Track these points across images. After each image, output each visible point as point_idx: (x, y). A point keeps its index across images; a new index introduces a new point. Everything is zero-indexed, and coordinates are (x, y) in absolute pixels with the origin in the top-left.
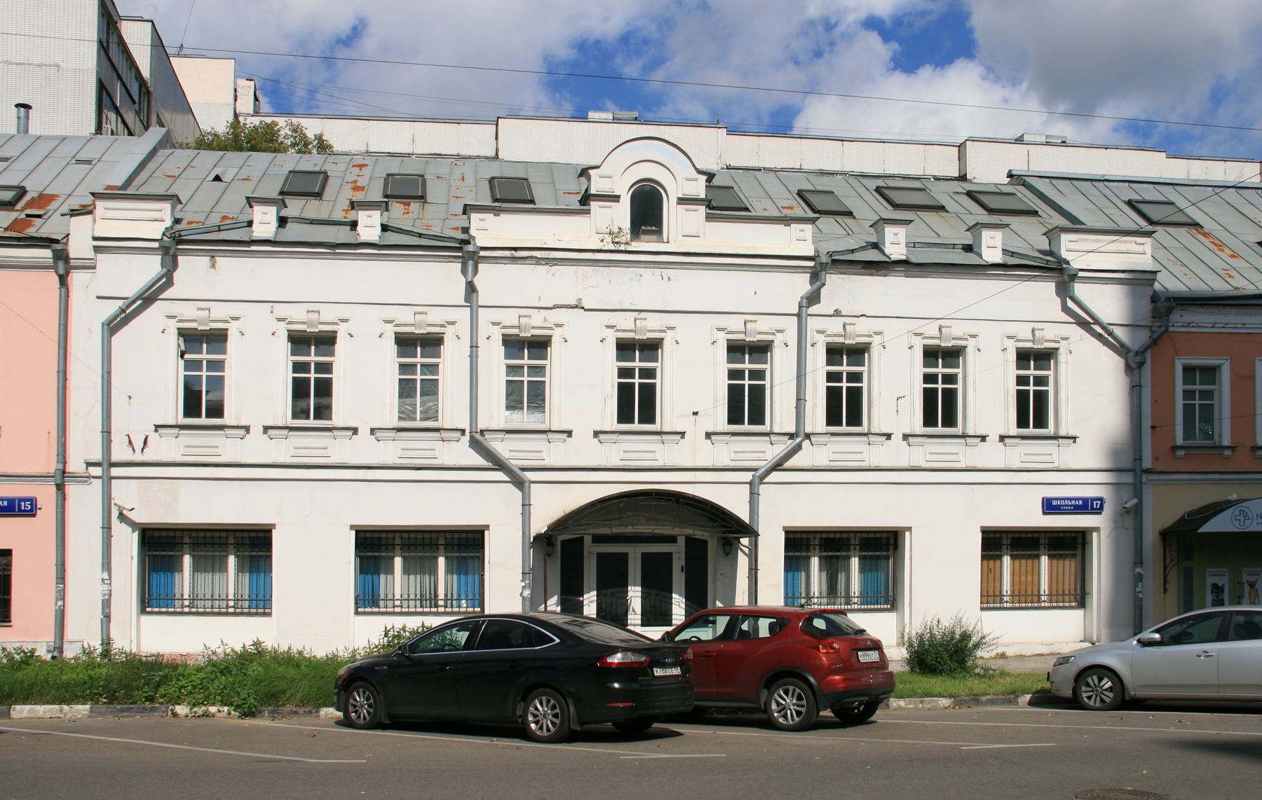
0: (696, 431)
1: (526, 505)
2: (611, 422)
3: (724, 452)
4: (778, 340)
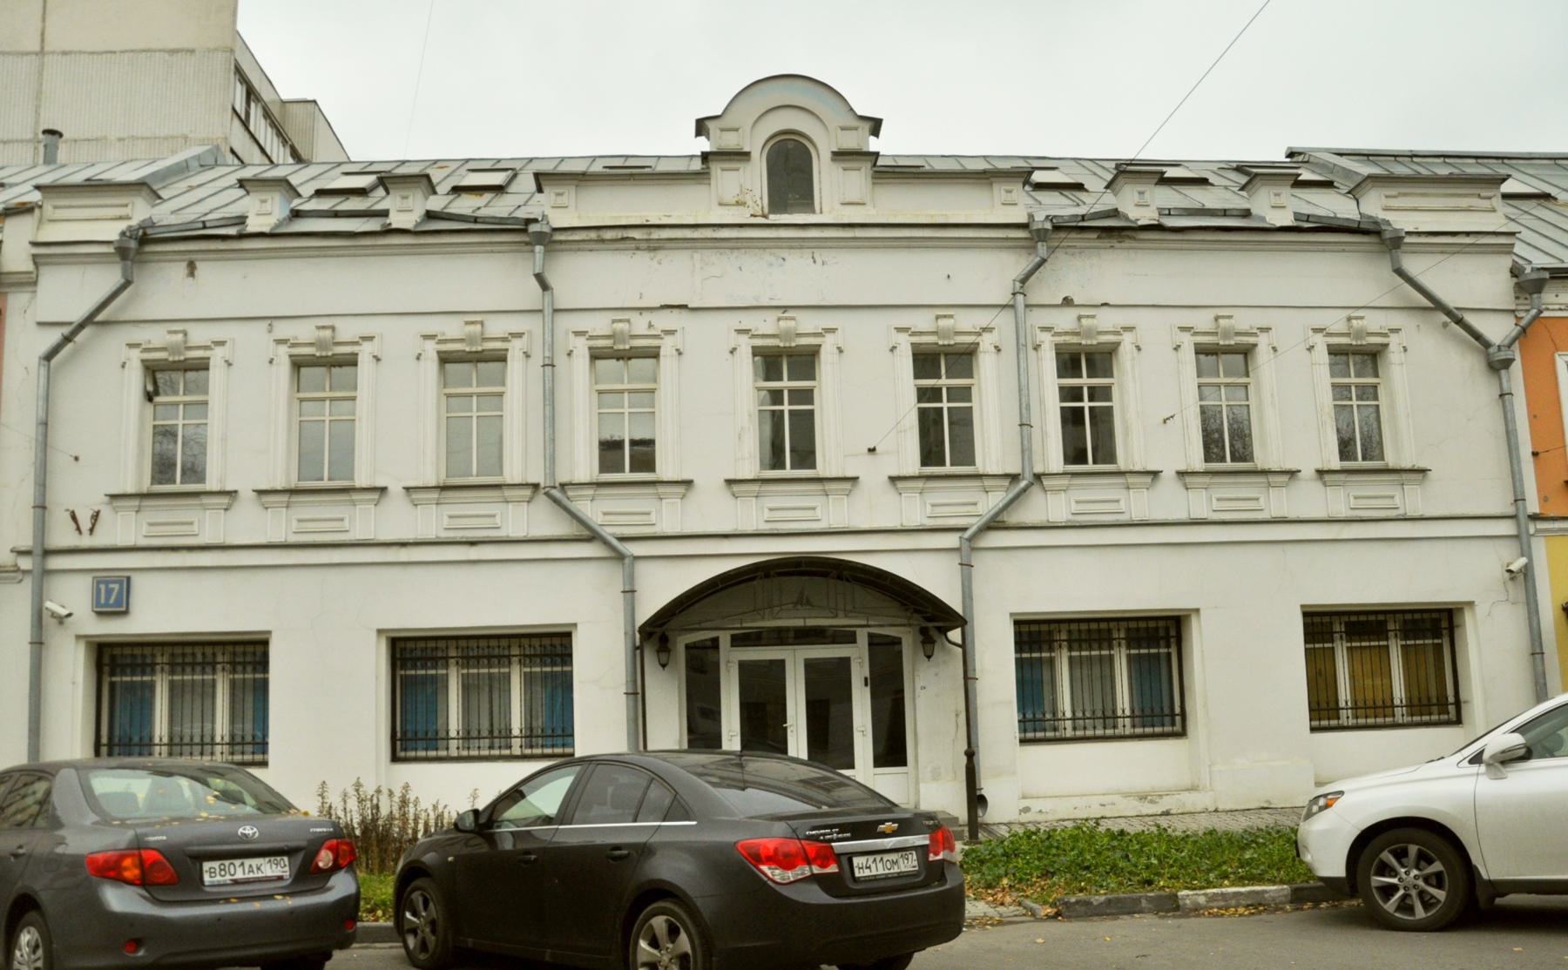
0: (873, 475)
1: (630, 592)
3: (914, 509)
4: (986, 342)
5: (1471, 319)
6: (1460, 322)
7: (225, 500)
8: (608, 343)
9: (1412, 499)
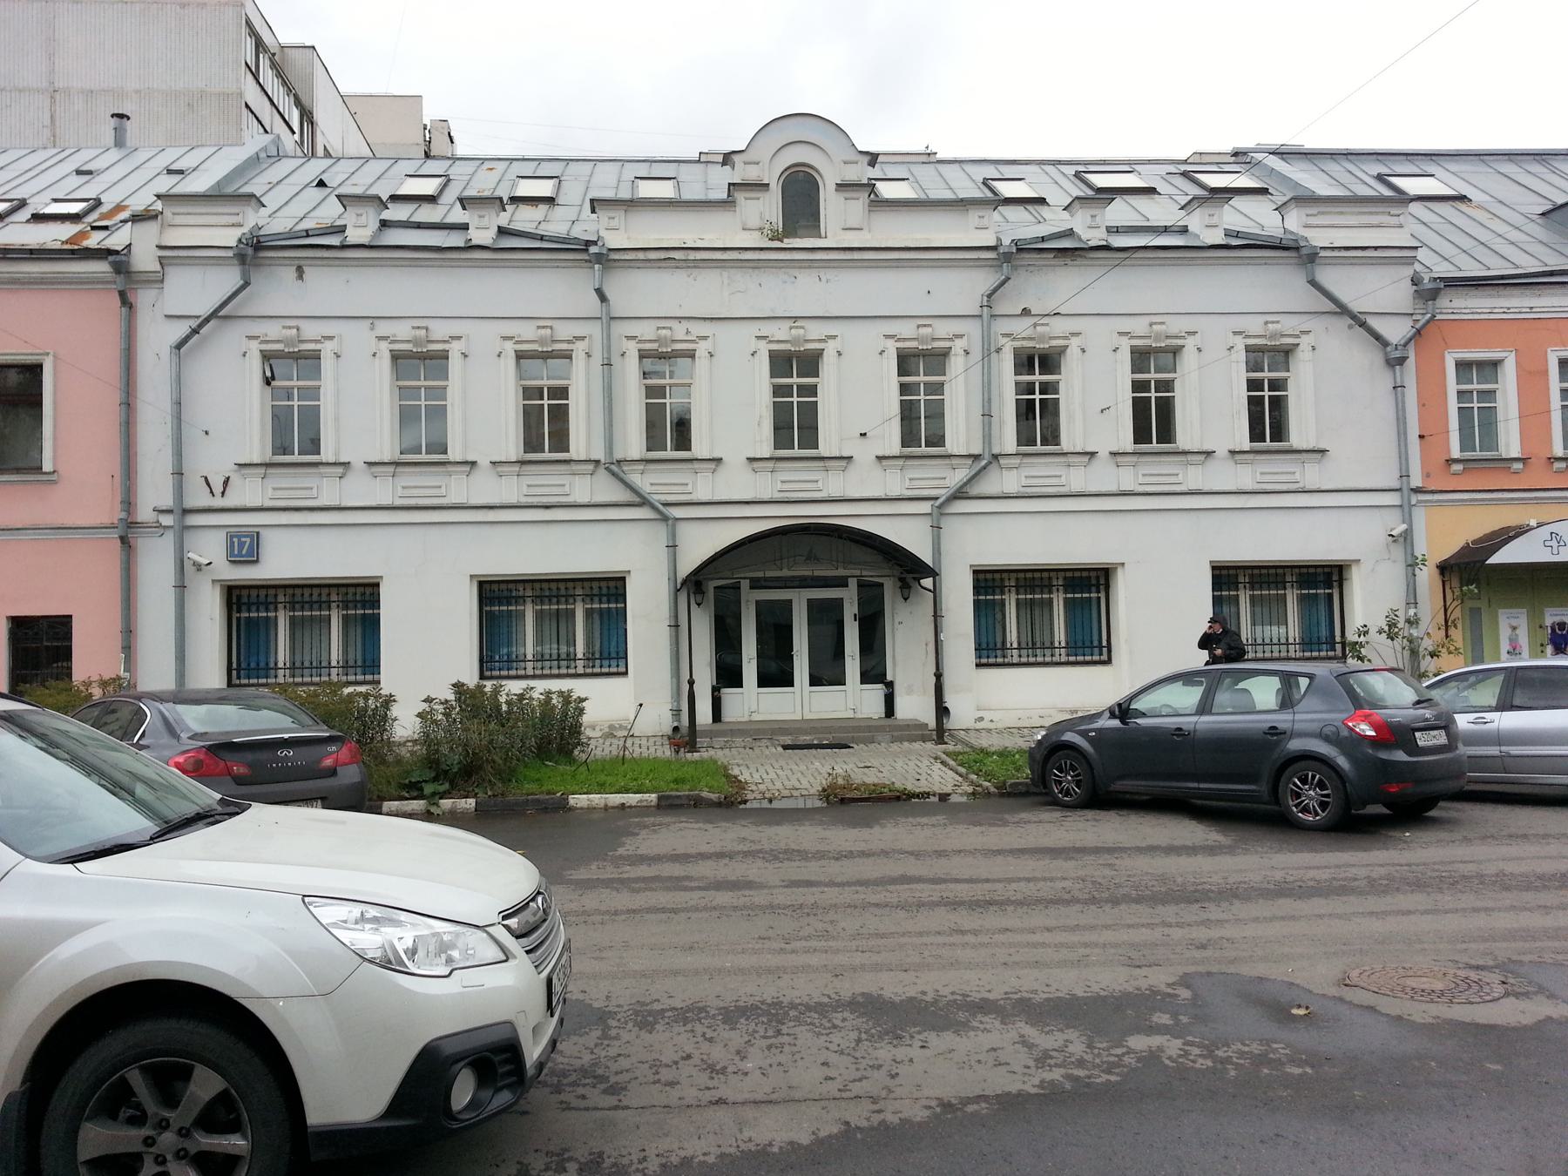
0: (864, 454)
1: (673, 547)
2: (766, 449)
3: (894, 482)
4: (958, 346)
5: (1374, 322)
6: (1363, 324)
7: (340, 470)
8: (654, 346)
9: (1311, 474)
